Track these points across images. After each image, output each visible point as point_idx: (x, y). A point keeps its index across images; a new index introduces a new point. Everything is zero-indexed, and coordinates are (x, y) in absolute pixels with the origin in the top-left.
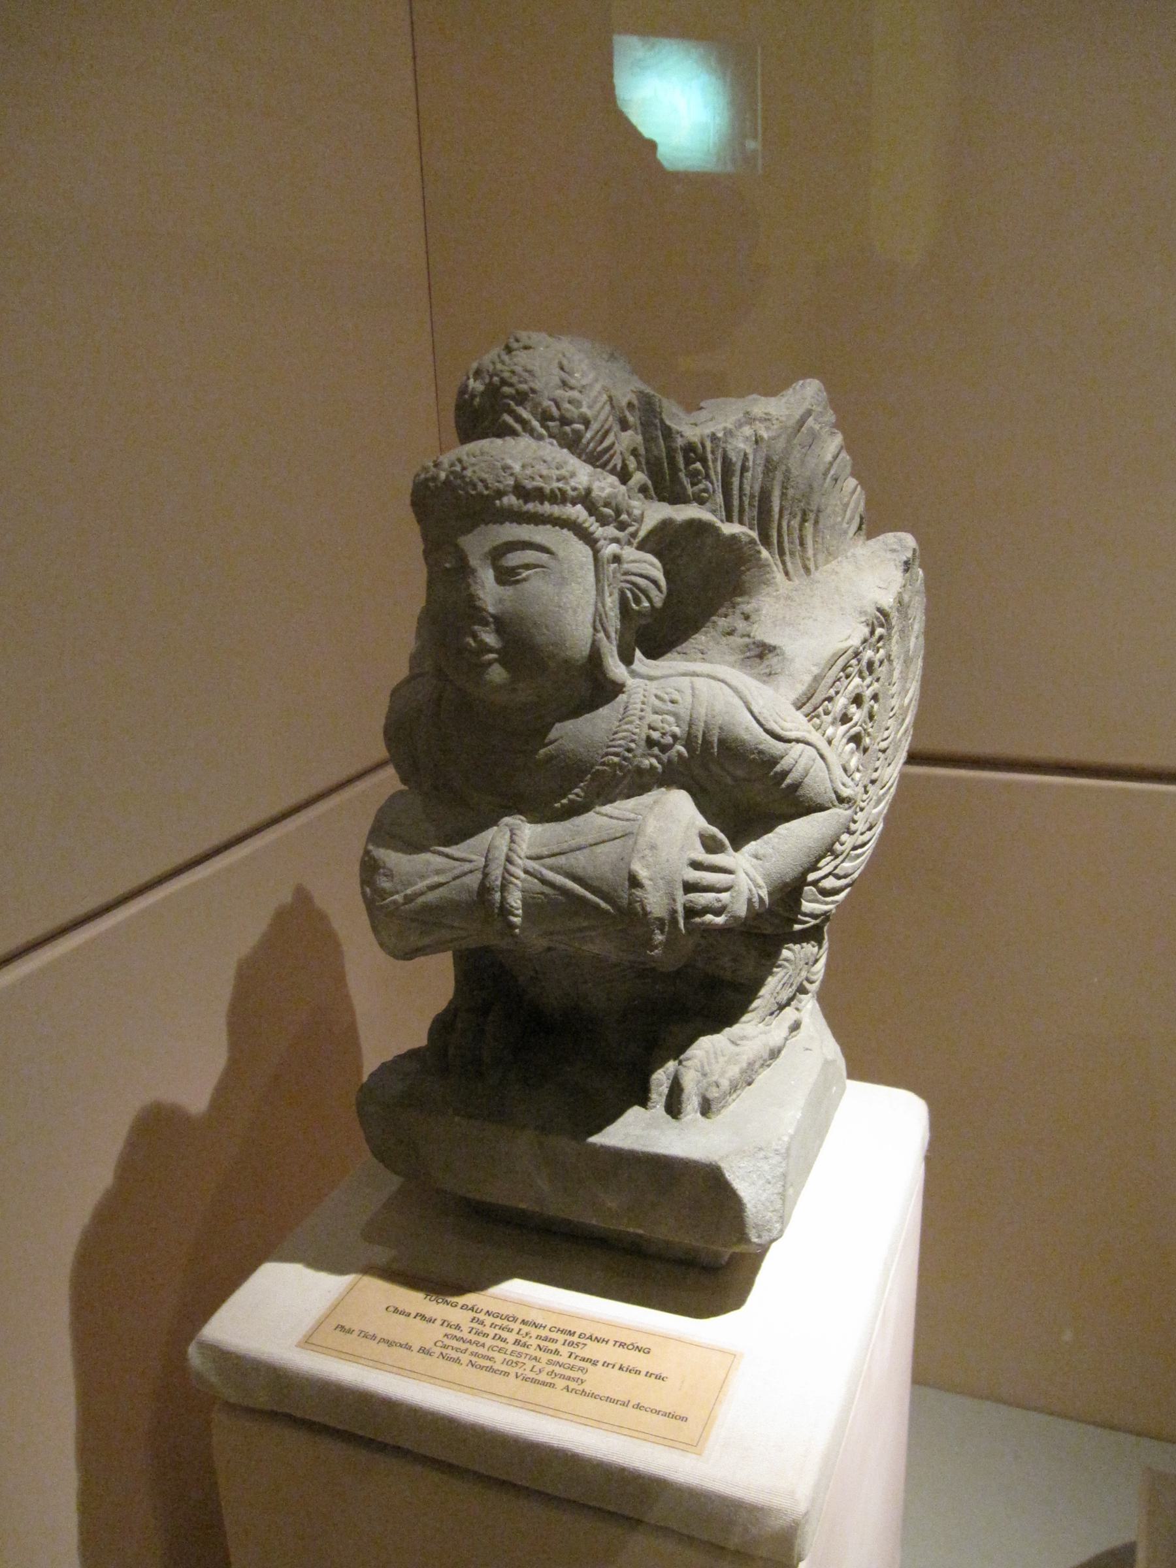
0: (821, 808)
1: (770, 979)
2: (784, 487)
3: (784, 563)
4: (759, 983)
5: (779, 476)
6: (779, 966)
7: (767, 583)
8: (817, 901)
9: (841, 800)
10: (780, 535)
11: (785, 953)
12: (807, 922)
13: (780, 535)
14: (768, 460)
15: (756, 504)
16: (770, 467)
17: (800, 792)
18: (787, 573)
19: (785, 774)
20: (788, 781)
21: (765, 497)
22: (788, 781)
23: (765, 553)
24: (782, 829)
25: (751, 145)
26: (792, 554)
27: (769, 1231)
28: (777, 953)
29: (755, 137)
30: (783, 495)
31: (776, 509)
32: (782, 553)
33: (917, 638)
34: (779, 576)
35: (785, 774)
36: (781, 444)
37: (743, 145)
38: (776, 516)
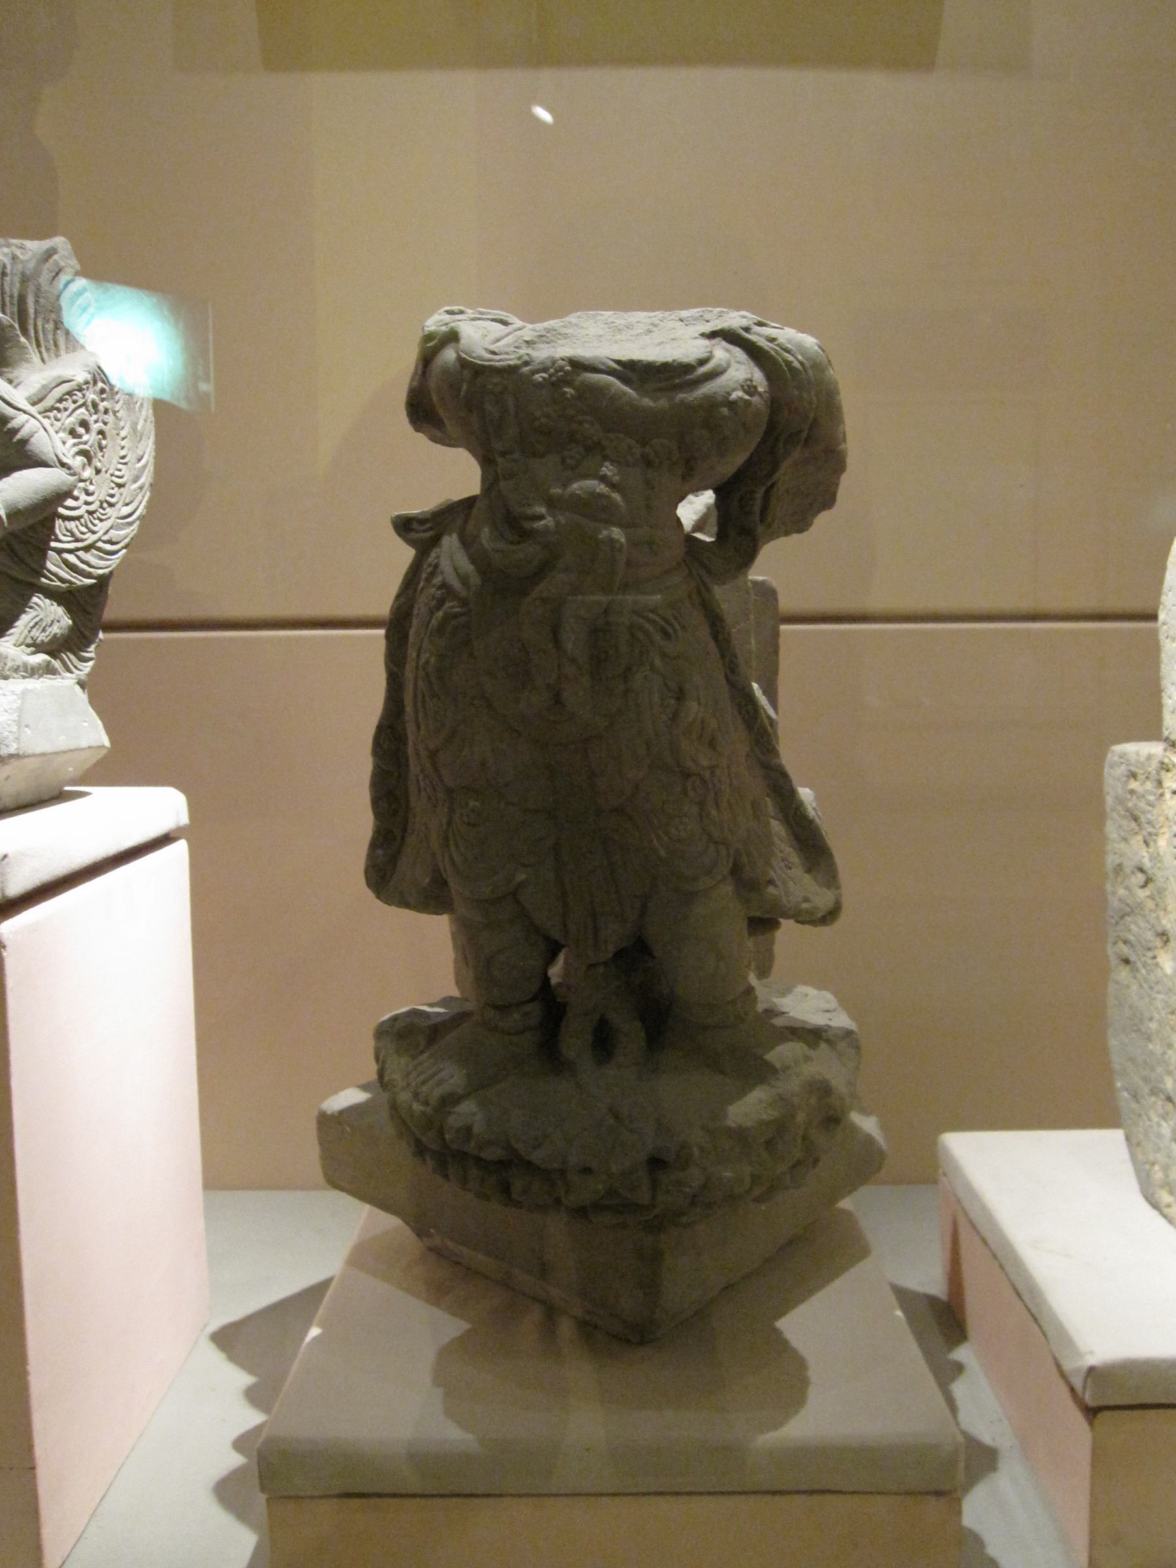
0: (44, 464)
1: (23, 616)
2: (37, 296)
3: (40, 353)
4: (16, 618)
5: (31, 289)
6: (31, 608)
7: (27, 361)
8: (59, 567)
9: (63, 465)
10: (36, 332)
11: (35, 599)
12: (52, 580)
13: (36, 332)
14: (23, 274)
15: (16, 303)
16: (25, 279)
17: (28, 447)
18: (43, 360)
19: (15, 431)
20: (18, 437)
21: (22, 300)
22: (18, 437)
23: (23, 339)
24: (16, 475)
25: (204, 387)
26: (48, 350)
27: (7, 746)
28: (30, 598)
29: (207, 380)
30: (37, 302)
31: (31, 311)
32: (38, 345)
33: (145, 421)
34: (35, 358)
35: (15, 431)
36: (31, 265)
37: (195, 387)
38: (32, 316)
